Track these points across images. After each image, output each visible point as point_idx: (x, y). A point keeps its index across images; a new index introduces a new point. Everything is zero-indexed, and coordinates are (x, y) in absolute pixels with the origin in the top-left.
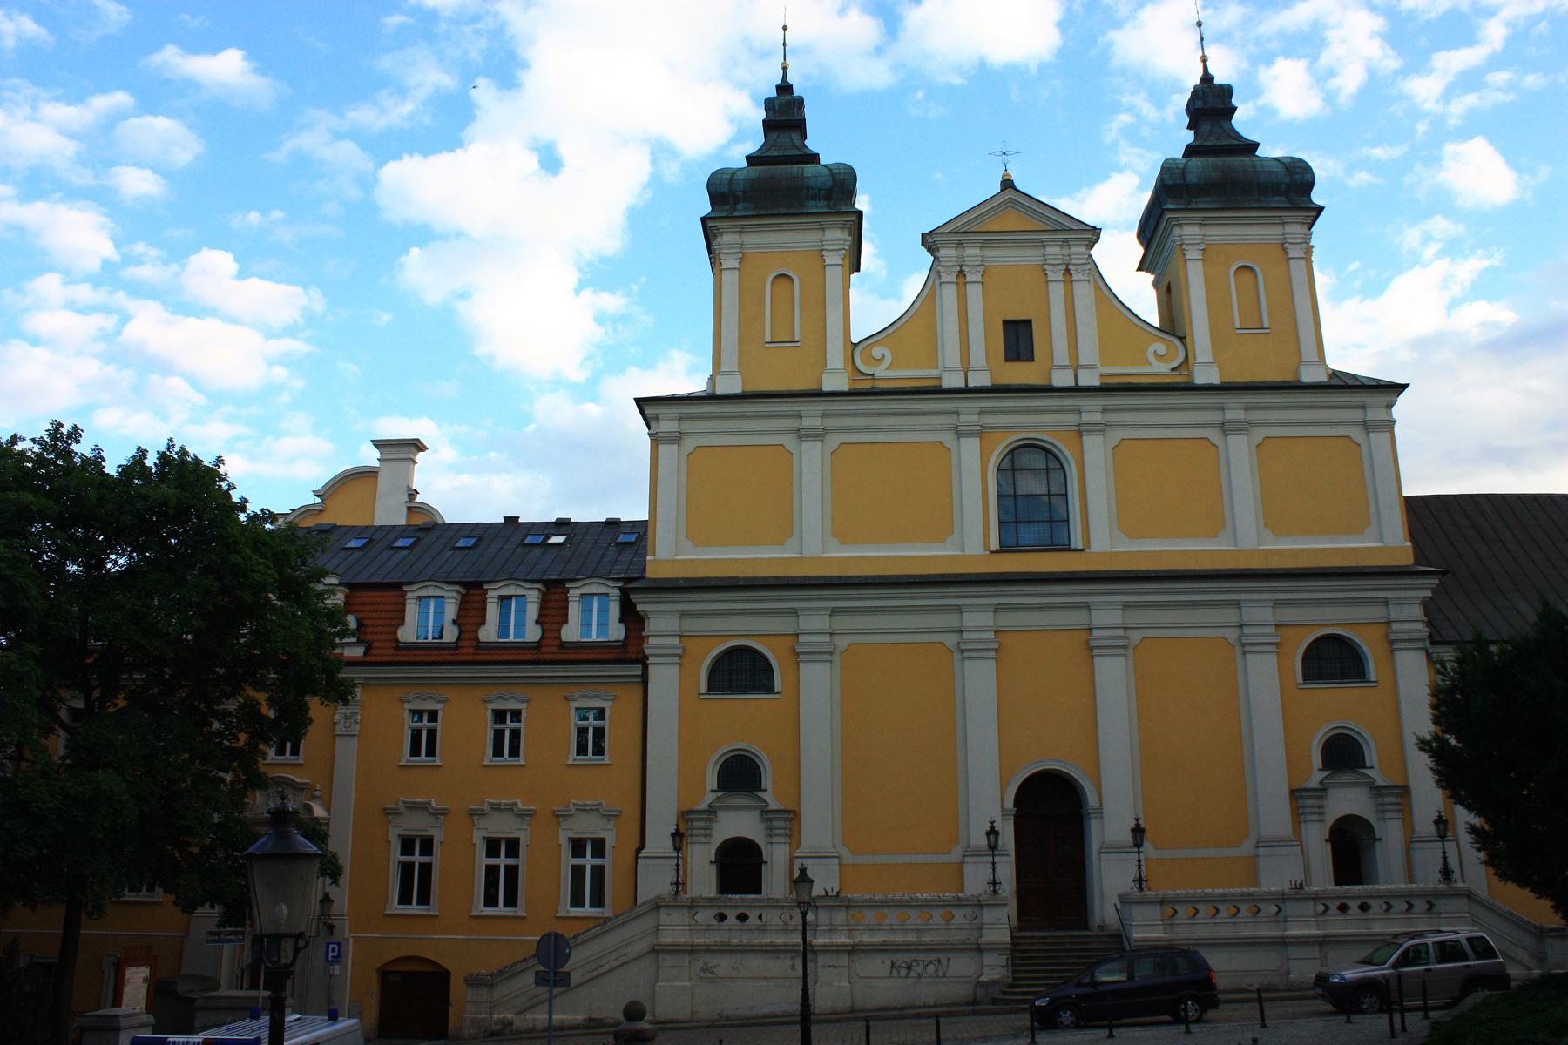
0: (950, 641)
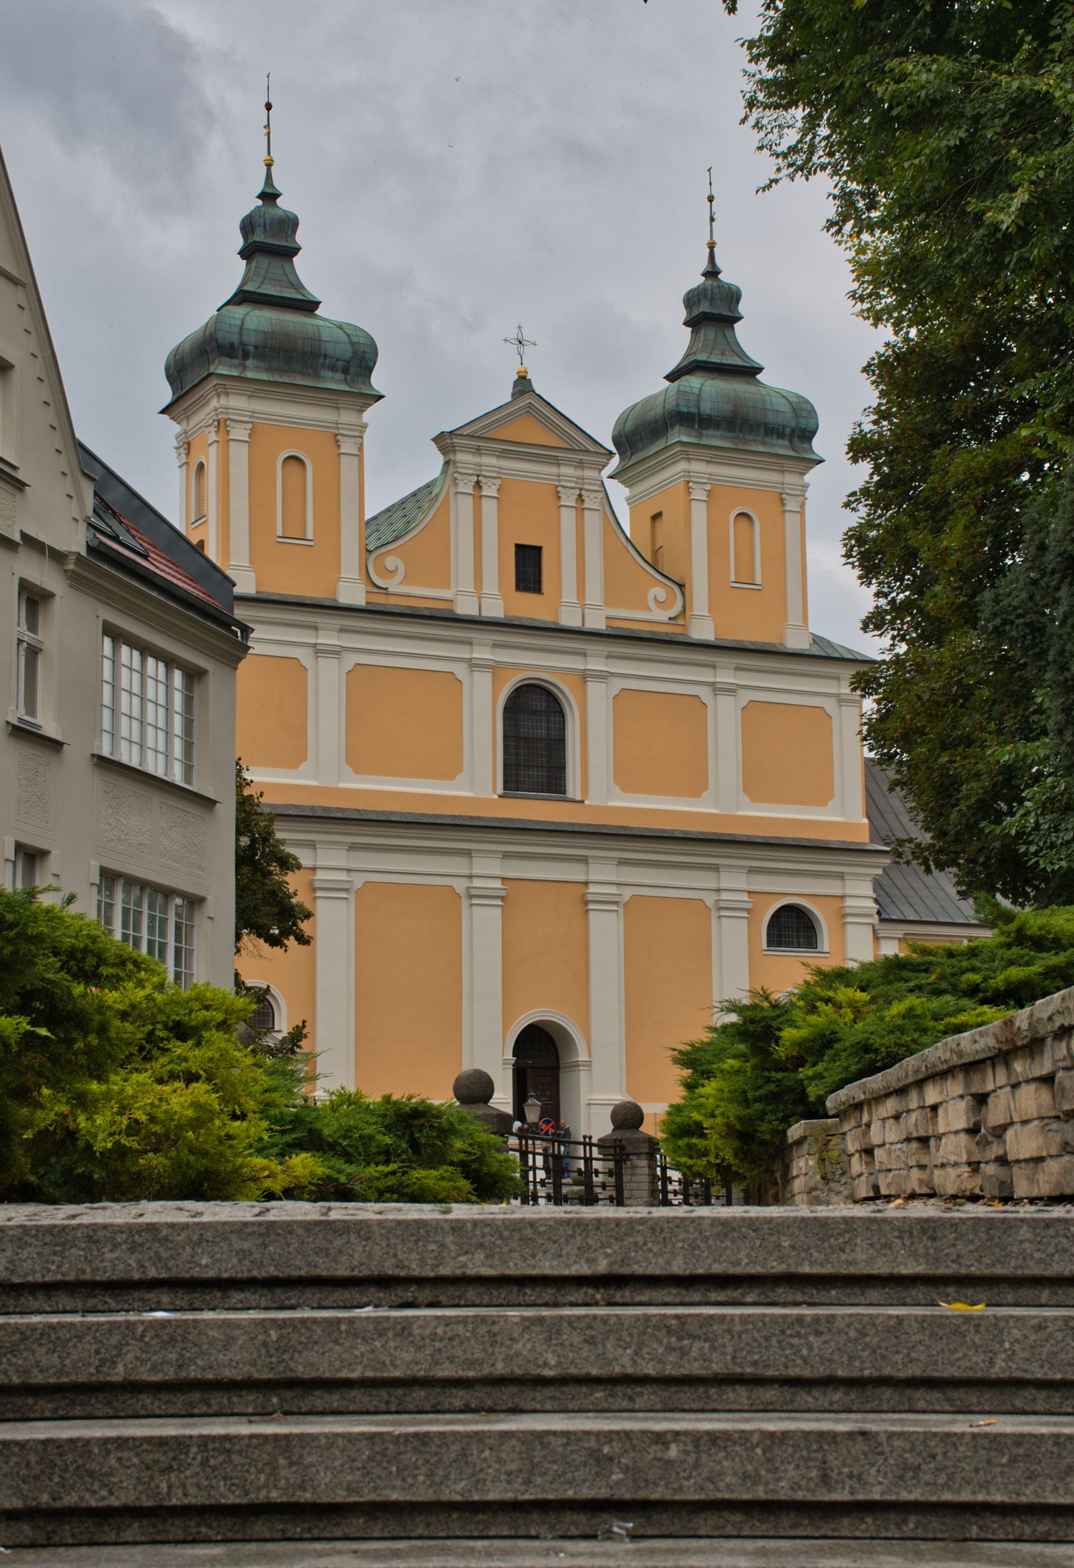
0: (460, 885)
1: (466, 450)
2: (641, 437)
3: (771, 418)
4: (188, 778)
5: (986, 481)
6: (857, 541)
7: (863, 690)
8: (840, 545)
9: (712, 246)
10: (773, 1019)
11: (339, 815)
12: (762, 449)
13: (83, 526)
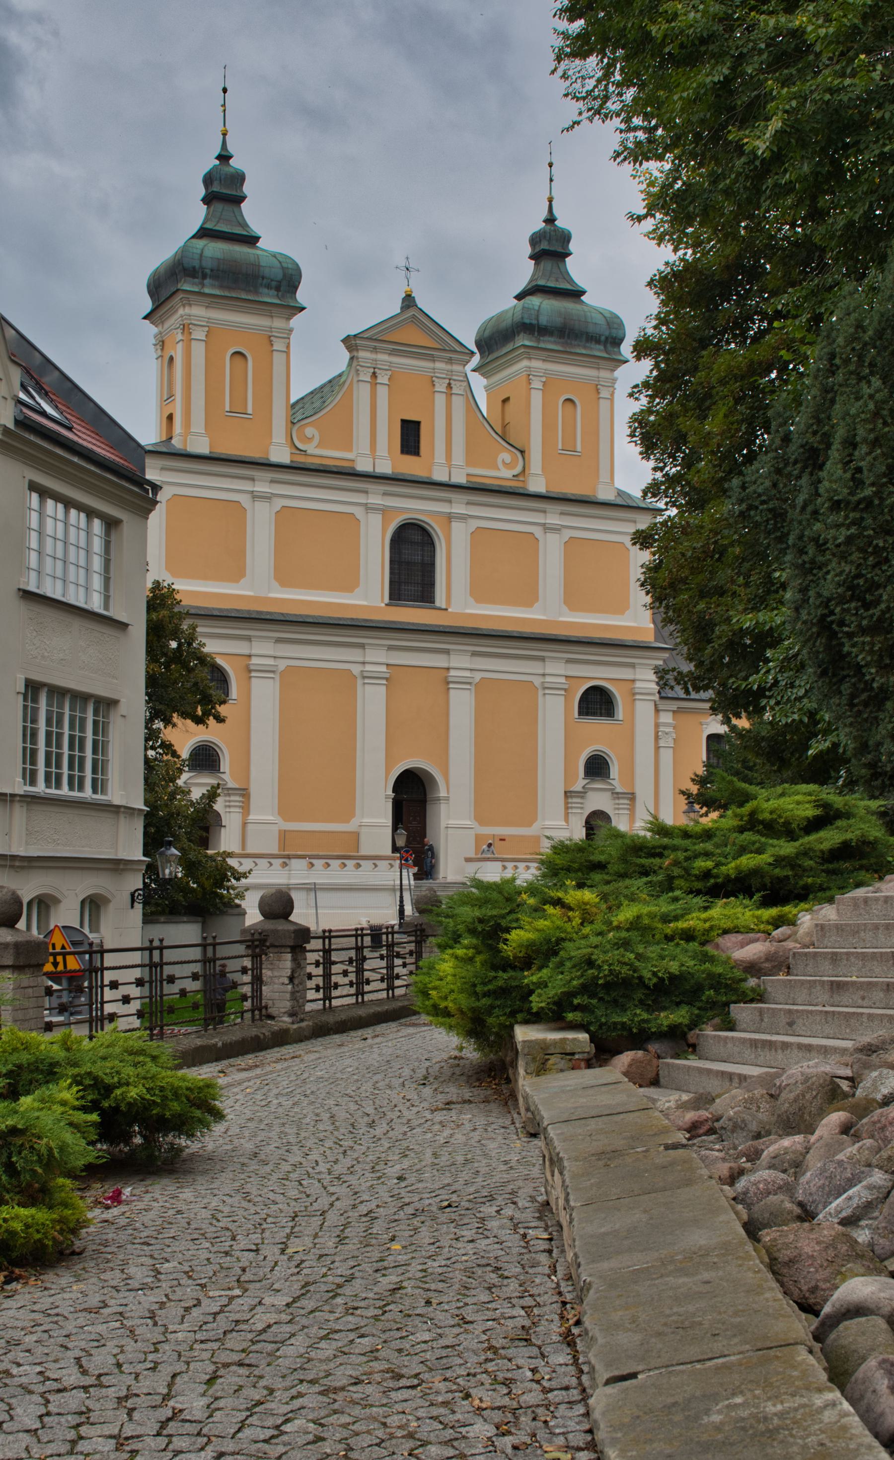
0: (356, 669)
1: (366, 348)
2: (495, 342)
3: (591, 329)
4: (106, 607)
5: (743, 378)
6: (640, 423)
7: (641, 544)
8: (626, 427)
9: (550, 200)
10: (503, 917)
11: (268, 617)
12: (584, 352)
13: (11, 404)
